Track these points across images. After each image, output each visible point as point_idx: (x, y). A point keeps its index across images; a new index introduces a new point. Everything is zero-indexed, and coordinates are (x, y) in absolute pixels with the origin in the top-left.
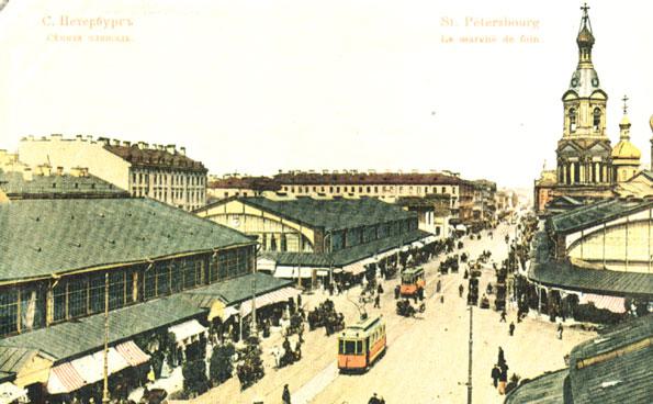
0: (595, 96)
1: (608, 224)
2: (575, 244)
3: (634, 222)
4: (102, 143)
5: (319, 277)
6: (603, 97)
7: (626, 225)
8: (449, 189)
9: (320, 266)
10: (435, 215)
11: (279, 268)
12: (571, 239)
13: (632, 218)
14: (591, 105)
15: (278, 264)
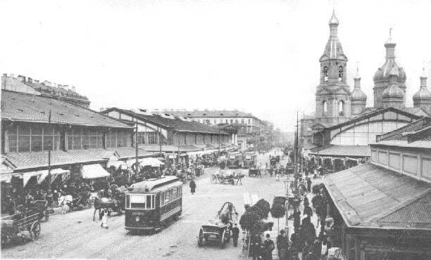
4: (22, 79)
7: (367, 123)
8: (246, 120)
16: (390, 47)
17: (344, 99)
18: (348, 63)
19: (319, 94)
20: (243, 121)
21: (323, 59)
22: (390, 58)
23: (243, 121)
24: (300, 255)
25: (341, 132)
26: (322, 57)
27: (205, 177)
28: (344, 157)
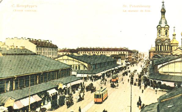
0: (166, 27)
1: (169, 62)
2: (160, 68)
3: (177, 62)
4: (28, 40)
5: (89, 77)
6: (168, 27)
7: (174, 62)
8: (125, 52)
9: (89, 74)
10: (121, 60)
11: (78, 74)
12: (159, 66)
13: (176, 60)
14: (165, 29)
15: (77, 73)
24: (26, 111)
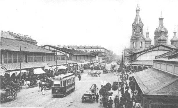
4: (9, 33)
7: (152, 51)
8: (102, 50)
16: (161, 19)
17: (142, 41)
18: (144, 26)
19: (132, 39)
20: (100, 50)
21: (133, 25)
22: (161, 24)
23: (100, 50)
24: (124, 106)
25: (141, 55)
26: (133, 24)
27: (85, 74)
28: (142, 65)
